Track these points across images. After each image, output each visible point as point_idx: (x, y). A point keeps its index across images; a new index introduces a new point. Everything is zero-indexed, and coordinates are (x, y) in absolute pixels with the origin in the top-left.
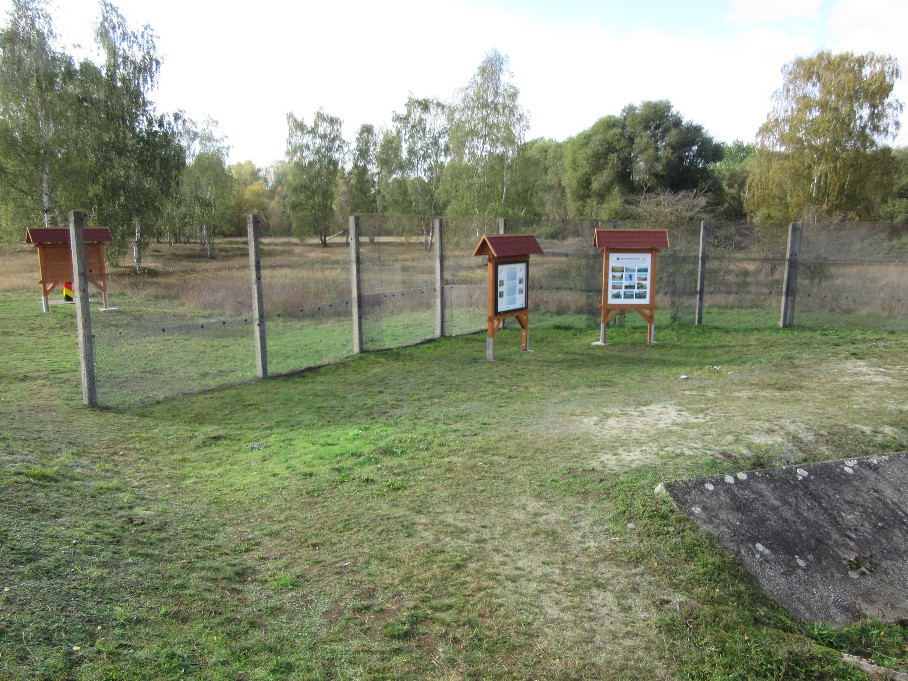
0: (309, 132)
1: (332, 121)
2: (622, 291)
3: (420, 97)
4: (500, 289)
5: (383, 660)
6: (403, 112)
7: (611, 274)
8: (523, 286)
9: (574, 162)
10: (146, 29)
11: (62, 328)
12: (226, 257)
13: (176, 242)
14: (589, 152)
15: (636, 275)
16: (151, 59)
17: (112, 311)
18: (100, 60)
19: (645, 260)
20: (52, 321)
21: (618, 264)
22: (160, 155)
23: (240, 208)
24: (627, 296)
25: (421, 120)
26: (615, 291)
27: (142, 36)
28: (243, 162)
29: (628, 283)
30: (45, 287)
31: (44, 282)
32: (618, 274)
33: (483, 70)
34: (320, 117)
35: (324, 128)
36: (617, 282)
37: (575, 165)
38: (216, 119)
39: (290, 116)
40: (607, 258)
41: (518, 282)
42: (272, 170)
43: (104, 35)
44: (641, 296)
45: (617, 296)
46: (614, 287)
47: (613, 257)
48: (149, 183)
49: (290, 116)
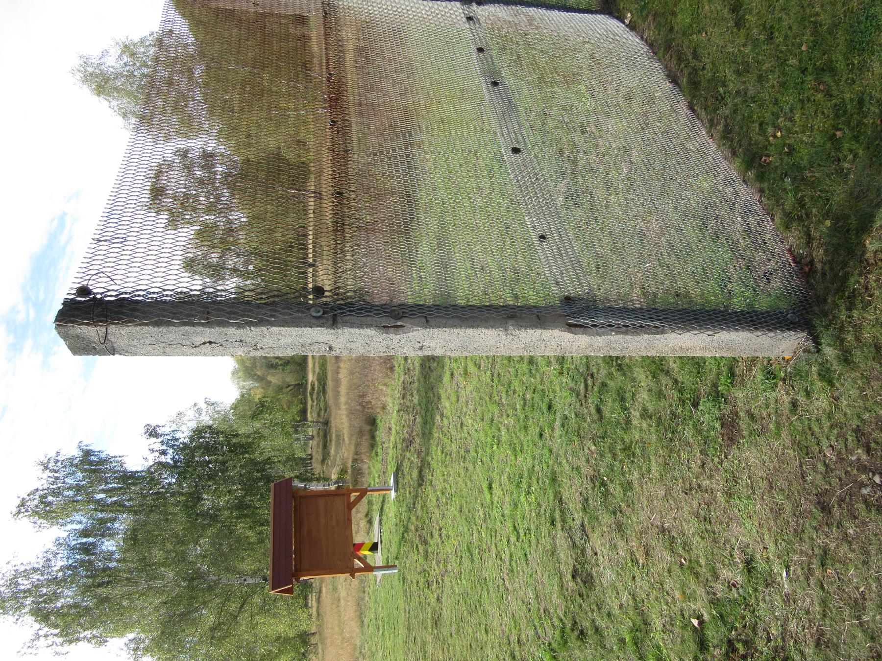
3: (146, 197)
5: (529, 493)
6: (164, 217)
11: (425, 542)
12: (326, 410)
17: (396, 482)
20: (414, 558)
25: (174, 197)
27: (56, 472)
30: (360, 570)
31: (352, 572)
38: (174, 415)
42: (242, 383)
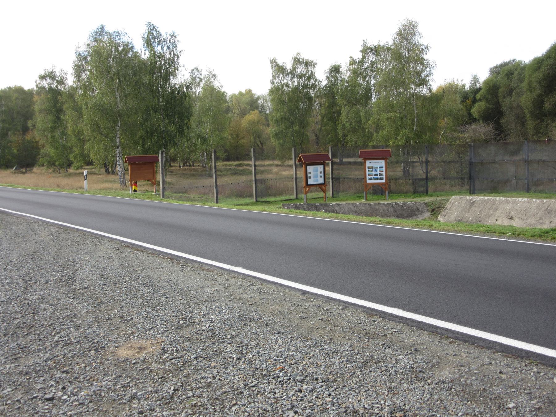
0: (289, 74)
1: (308, 64)
2: (373, 177)
4: (308, 175)
7: (367, 170)
8: (322, 175)
9: (530, 84)
10: (172, 37)
13: (184, 166)
14: (540, 75)
15: (378, 169)
16: (174, 55)
18: (145, 55)
19: (382, 163)
21: (370, 165)
22: (177, 106)
23: (238, 135)
24: (375, 179)
26: (370, 177)
28: (243, 91)
29: (375, 173)
30: (131, 183)
32: (371, 170)
33: (400, 34)
34: (297, 61)
35: (300, 69)
36: (370, 173)
37: (531, 88)
39: (274, 62)
40: (365, 162)
41: (319, 172)
43: (149, 43)
44: (381, 179)
45: (371, 179)
46: (369, 175)
47: (368, 162)
48: (172, 129)
49: (274, 62)
